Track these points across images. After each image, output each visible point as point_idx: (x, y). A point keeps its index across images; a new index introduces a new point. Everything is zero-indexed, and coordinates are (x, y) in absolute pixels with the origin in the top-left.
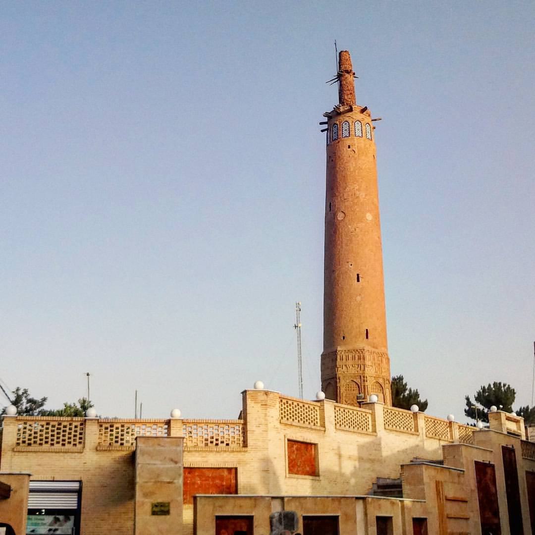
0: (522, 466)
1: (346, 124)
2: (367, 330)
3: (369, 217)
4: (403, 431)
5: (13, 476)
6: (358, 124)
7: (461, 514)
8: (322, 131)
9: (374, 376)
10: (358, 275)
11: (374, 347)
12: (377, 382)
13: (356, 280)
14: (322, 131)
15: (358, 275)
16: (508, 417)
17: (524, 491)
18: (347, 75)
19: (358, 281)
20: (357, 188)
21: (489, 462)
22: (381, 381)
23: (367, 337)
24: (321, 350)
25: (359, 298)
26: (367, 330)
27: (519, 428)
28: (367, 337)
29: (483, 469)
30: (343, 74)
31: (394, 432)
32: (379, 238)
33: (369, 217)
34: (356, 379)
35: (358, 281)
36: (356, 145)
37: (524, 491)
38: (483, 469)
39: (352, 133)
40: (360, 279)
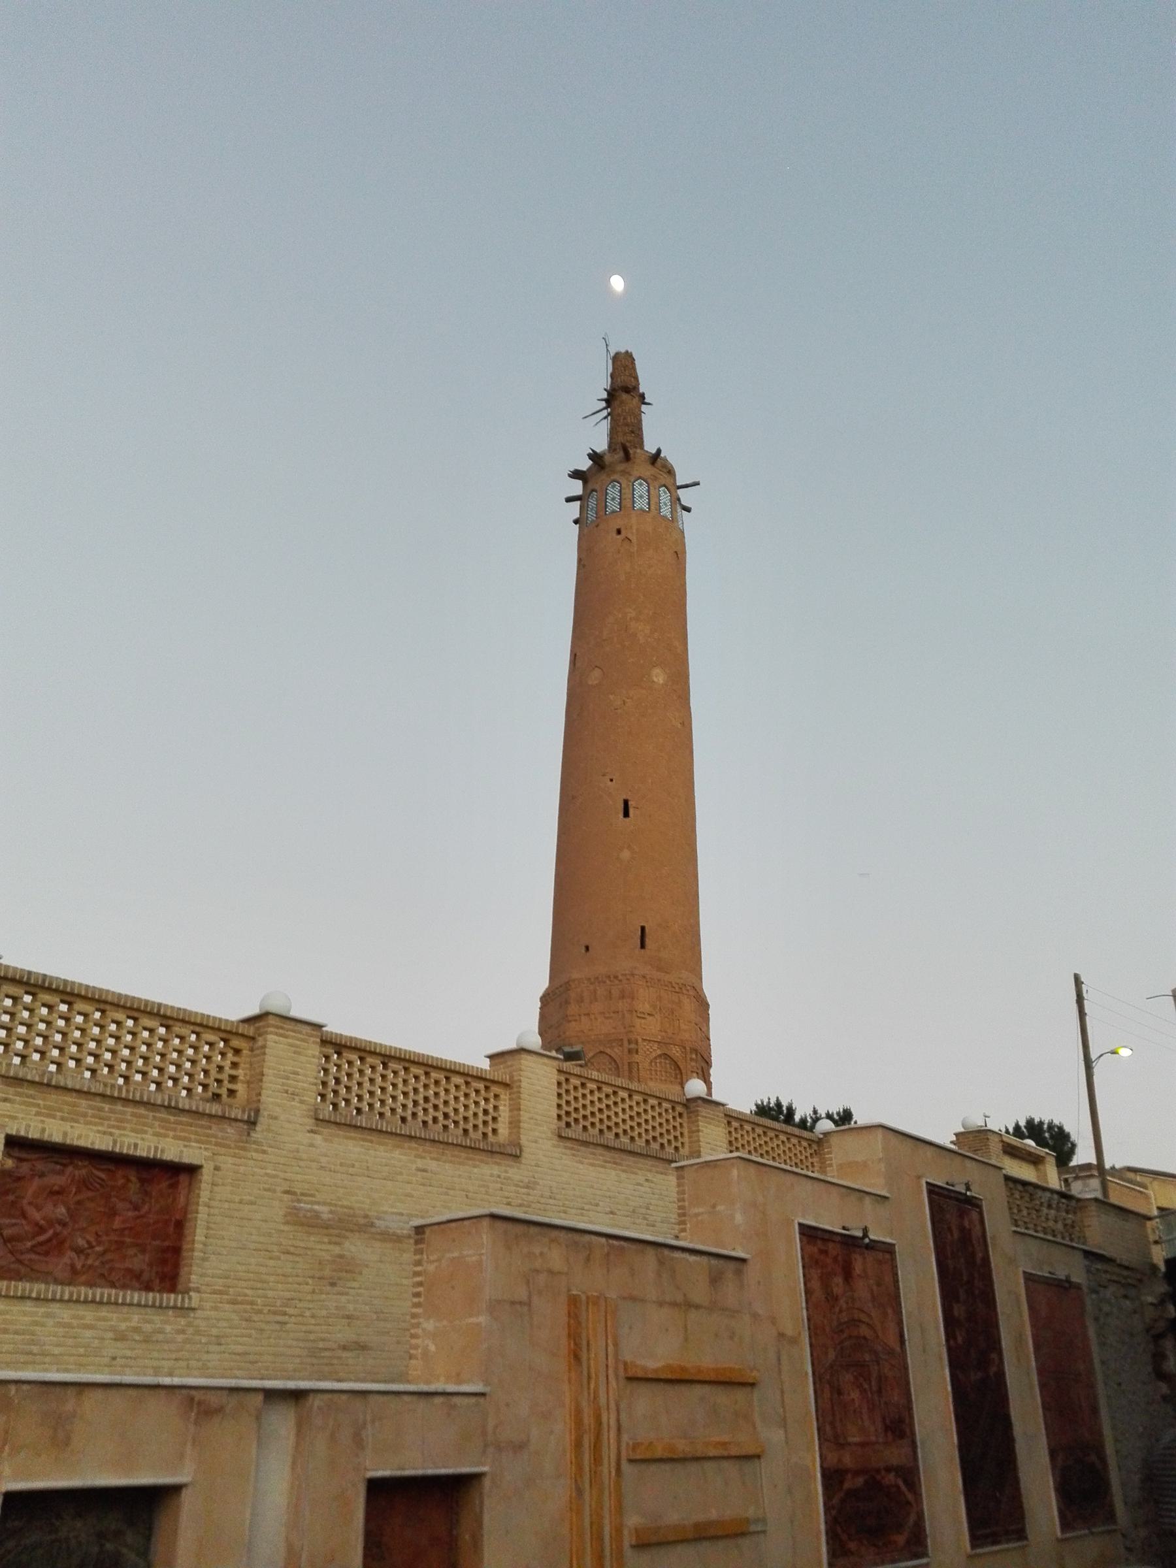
0: (1013, 1263)
1: (614, 487)
2: (643, 928)
3: (659, 677)
4: (611, 1144)
5: (122, 1391)
6: (641, 485)
7: (707, 1359)
8: (569, 500)
9: (659, 1038)
10: (626, 803)
11: (659, 969)
12: (666, 1056)
13: (621, 815)
14: (569, 500)
15: (626, 803)
16: (1009, 1145)
17: (1020, 1339)
18: (625, 396)
19: (626, 814)
20: (633, 614)
21: (865, 1231)
22: (676, 1052)
23: (643, 946)
24: (541, 982)
25: (626, 854)
26: (643, 928)
27: (1044, 1176)
28: (643, 946)
29: (835, 1257)
30: (623, 393)
31: (600, 1151)
32: (683, 724)
33: (659, 677)
34: (612, 1047)
35: (626, 814)
36: (635, 528)
37: (1020, 1339)
38: (835, 1257)
39: (628, 503)
40: (631, 811)
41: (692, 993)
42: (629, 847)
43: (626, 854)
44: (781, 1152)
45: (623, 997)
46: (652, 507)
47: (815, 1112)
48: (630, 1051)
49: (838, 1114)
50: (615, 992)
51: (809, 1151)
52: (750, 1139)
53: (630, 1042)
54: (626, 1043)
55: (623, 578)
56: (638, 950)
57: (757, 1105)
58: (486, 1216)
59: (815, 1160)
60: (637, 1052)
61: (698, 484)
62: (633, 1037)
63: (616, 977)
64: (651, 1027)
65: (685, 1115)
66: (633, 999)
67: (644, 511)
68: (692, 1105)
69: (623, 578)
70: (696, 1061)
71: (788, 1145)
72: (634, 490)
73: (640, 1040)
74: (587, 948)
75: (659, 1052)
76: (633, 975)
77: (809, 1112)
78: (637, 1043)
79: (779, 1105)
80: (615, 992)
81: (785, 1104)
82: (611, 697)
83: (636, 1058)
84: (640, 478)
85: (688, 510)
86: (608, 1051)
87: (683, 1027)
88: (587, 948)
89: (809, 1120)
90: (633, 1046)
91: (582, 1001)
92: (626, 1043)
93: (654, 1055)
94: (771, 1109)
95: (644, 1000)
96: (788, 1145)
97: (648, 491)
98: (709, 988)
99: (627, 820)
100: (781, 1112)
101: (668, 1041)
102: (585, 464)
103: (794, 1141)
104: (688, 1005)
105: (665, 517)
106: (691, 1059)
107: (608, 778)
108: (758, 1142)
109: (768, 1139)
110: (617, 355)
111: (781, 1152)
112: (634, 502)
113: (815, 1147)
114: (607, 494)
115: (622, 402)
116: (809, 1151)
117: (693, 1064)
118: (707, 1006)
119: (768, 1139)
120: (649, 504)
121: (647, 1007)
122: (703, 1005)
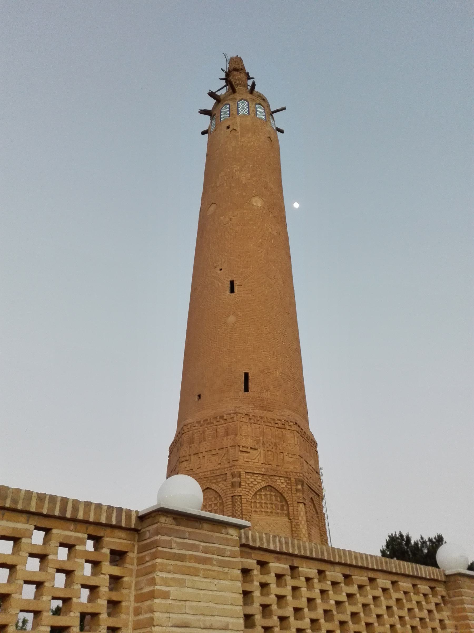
2: (246, 375)
6: (243, 103)
10: (232, 283)
12: (270, 487)
15: (232, 283)
18: (235, 73)
19: (232, 291)
22: (281, 484)
23: (246, 389)
25: (232, 319)
26: (246, 375)
28: (246, 389)
34: (217, 483)
35: (232, 291)
41: (295, 428)
42: (234, 313)
43: (232, 319)
44: (382, 610)
45: (227, 435)
46: (251, 112)
47: (422, 538)
48: (233, 485)
49: (435, 538)
50: (221, 430)
51: (433, 600)
52: (316, 593)
53: (233, 476)
54: (229, 476)
55: (231, 150)
56: (242, 393)
57: (389, 536)
58: (191, 628)
59: (445, 614)
60: (240, 485)
61: (284, 109)
62: (235, 470)
63: (222, 417)
64: (256, 460)
65: (133, 556)
66: (236, 435)
67: (245, 115)
68: (149, 530)
69: (231, 150)
70: (303, 492)
71: (395, 595)
72: (238, 105)
73: (243, 473)
74: (199, 396)
75: (263, 484)
76: (236, 413)
77: (419, 538)
78: (240, 476)
79: (401, 535)
80: (221, 430)
81: (405, 534)
82: (222, 218)
83: (239, 491)
84: (242, 99)
85: (282, 131)
86: (214, 487)
87: (287, 459)
88: (199, 396)
89: (420, 543)
90: (236, 479)
91: (193, 442)
92: (229, 476)
93: (258, 487)
94: (397, 538)
95: (247, 434)
96: (395, 595)
97: (248, 105)
98: (316, 427)
99: (233, 294)
100: (403, 540)
101: (272, 473)
102: (210, 104)
103: (405, 585)
104: (292, 440)
105: (261, 119)
106: (297, 490)
107: (218, 268)
108: (333, 597)
109: (354, 589)
110: (232, 59)
111: (382, 610)
112: (238, 111)
113: (441, 589)
114: (221, 112)
115: (234, 76)
116: (433, 600)
117: (300, 494)
118: (314, 444)
119: (354, 589)
120: (249, 111)
121: (250, 442)
122: (311, 444)
